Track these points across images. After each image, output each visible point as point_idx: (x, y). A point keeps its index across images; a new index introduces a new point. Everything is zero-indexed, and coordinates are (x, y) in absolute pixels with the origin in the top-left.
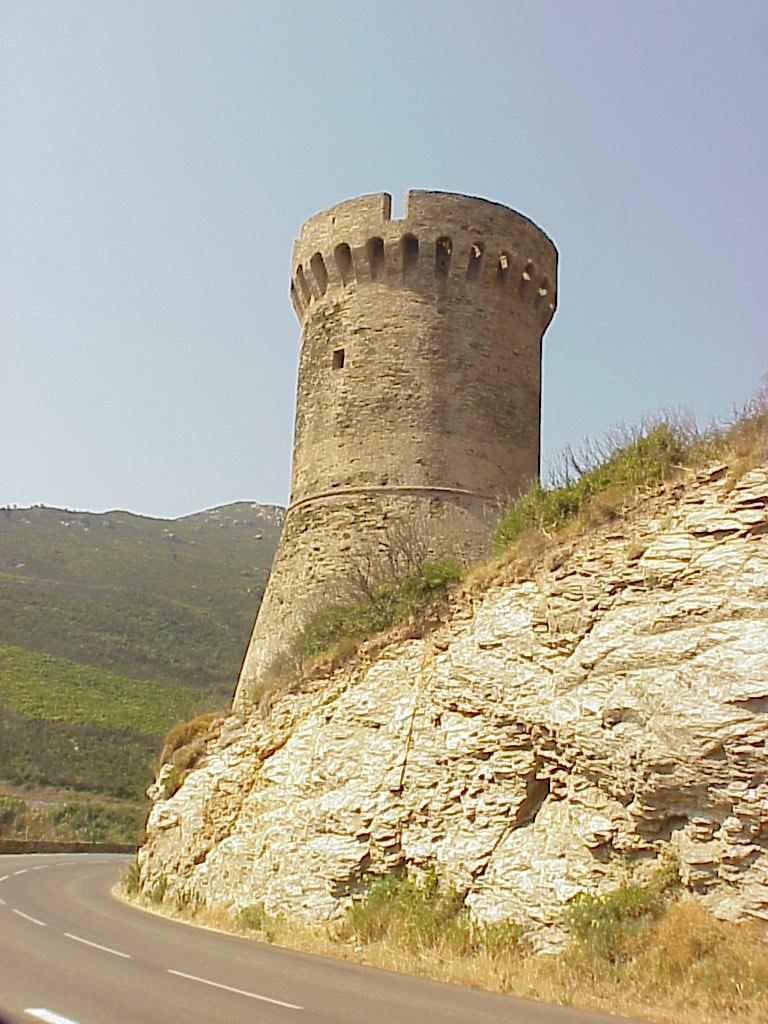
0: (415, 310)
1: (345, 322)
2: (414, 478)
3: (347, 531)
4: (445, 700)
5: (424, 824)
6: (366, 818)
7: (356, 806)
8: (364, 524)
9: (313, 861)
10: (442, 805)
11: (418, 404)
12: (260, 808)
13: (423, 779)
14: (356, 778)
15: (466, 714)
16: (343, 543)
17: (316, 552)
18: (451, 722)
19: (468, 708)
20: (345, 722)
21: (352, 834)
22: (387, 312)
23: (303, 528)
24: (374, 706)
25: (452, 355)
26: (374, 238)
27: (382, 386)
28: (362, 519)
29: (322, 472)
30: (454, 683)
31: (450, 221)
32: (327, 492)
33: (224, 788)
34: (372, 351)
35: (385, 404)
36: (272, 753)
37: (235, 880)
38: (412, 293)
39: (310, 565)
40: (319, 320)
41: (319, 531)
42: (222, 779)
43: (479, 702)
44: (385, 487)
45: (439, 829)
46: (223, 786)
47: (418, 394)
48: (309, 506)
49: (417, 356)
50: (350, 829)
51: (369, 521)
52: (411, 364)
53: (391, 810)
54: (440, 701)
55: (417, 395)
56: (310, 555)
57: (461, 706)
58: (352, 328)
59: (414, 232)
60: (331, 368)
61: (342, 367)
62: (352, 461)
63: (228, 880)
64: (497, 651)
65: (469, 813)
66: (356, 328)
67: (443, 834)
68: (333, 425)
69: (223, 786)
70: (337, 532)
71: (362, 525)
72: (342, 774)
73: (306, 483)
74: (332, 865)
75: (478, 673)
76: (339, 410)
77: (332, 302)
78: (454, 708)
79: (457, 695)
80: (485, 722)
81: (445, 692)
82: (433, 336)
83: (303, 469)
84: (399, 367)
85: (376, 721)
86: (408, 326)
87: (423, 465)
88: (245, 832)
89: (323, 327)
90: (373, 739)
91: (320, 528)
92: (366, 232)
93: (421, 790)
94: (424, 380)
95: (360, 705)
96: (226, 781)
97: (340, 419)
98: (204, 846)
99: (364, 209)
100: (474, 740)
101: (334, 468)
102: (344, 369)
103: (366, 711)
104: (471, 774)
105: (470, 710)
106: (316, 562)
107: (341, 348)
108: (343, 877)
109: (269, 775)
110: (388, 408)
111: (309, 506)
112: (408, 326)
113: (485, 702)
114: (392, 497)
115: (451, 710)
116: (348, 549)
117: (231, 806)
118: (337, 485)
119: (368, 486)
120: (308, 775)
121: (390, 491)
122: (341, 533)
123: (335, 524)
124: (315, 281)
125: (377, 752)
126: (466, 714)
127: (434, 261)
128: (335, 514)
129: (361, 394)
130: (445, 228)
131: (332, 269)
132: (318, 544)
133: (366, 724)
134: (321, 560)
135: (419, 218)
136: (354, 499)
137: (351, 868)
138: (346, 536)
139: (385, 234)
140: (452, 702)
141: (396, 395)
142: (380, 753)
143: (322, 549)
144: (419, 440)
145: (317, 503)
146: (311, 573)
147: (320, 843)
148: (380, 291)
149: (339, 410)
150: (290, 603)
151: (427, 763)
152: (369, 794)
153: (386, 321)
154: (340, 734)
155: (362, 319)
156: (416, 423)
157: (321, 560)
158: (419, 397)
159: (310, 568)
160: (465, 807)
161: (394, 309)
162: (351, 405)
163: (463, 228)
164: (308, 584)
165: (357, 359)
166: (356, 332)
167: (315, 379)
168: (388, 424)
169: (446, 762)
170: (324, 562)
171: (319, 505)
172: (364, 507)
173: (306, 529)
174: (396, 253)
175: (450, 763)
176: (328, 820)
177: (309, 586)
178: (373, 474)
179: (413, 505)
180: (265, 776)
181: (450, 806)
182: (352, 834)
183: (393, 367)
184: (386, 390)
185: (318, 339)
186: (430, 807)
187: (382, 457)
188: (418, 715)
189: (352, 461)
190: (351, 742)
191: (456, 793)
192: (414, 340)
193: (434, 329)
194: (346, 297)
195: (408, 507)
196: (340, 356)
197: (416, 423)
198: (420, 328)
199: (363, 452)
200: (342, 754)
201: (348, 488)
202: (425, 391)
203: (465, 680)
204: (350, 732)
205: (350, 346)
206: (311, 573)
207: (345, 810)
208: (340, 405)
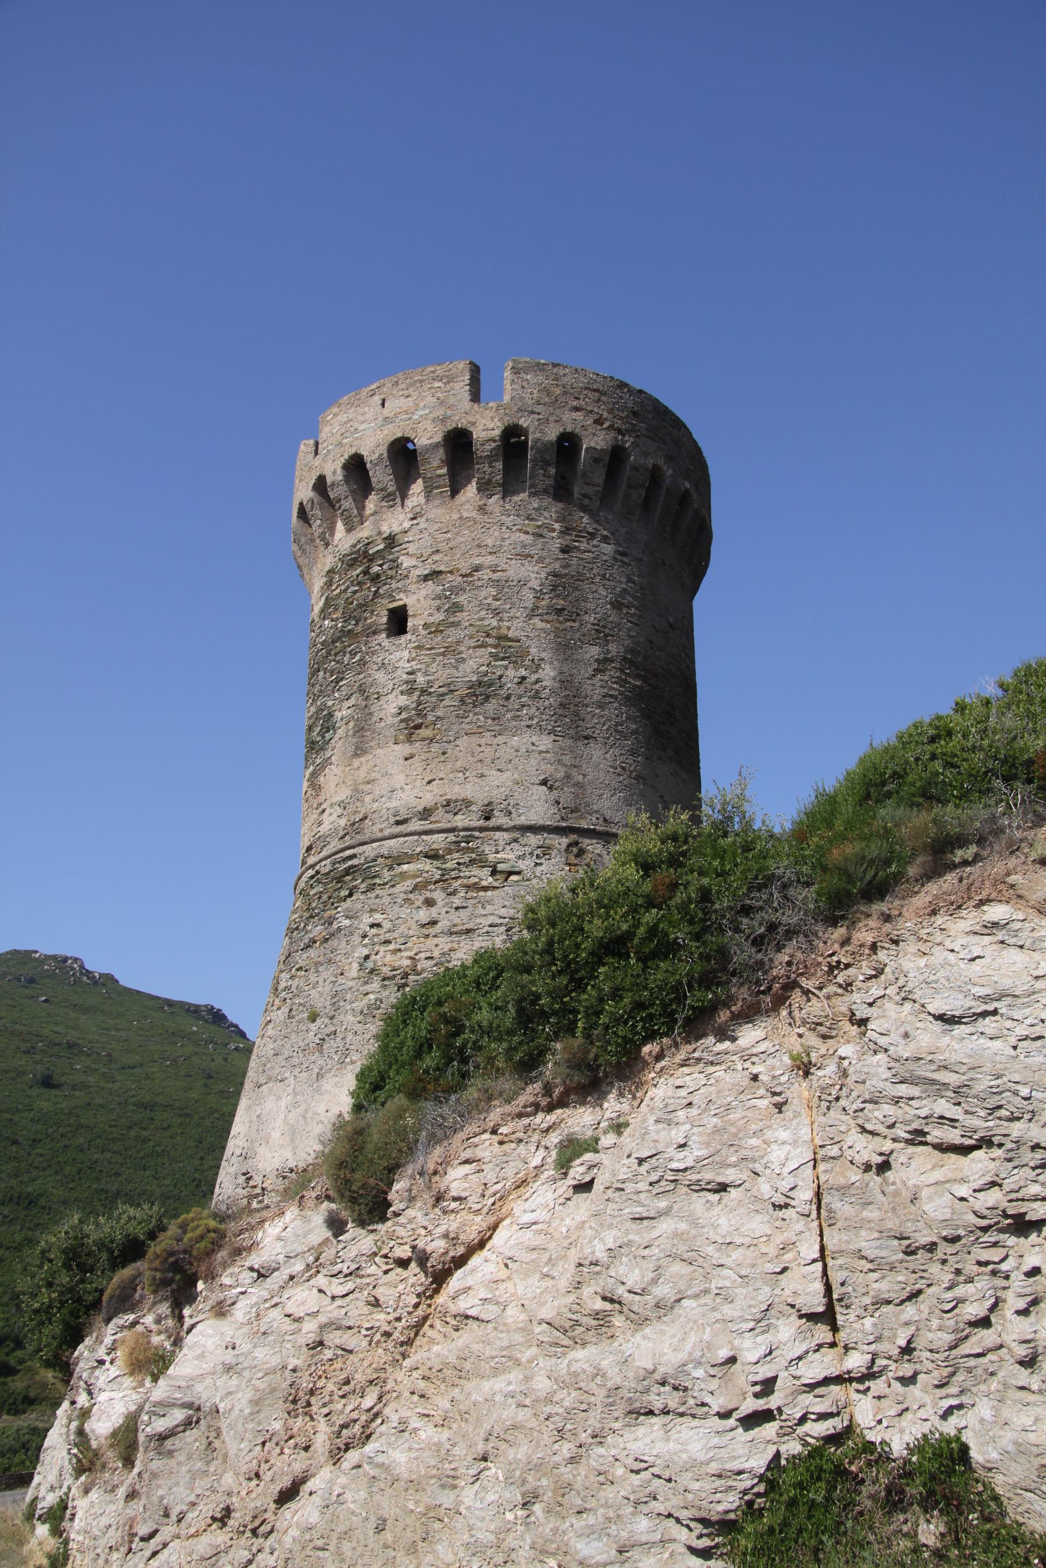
0: (524, 546)
1: (406, 562)
2: (537, 808)
3: (428, 894)
4: (892, 1126)
5: (908, 1381)
6: (759, 1378)
7: (724, 1353)
8: (459, 882)
9: (636, 1480)
10: (948, 1338)
11: (537, 692)
12: (459, 1372)
13: (883, 1286)
14: (696, 1296)
15: (943, 1148)
16: (424, 915)
17: (374, 931)
18: (917, 1168)
19: (953, 1136)
20: (643, 1186)
21: (725, 1415)
22: (479, 546)
23: (344, 893)
24: (704, 1153)
25: (586, 618)
26: (456, 429)
27: (474, 664)
28: (453, 874)
29: (375, 801)
30: (903, 1090)
31: (577, 409)
32: (387, 833)
33: (338, 1341)
34: (457, 608)
35: (481, 691)
36: (460, 1262)
37: (409, 1535)
38: (518, 520)
39: (365, 952)
40: (353, 563)
41: (377, 897)
42: (331, 1324)
43: (980, 1124)
44: (492, 823)
45: (953, 1390)
46: (334, 1338)
47: (537, 676)
48: (354, 856)
49: (530, 617)
50: (717, 1404)
51: (465, 877)
52: (523, 629)
53: (811, 1356)
54: (881, 1129)
55: (534, 677)
56: (364, 936)
57: (937, 1134)
58: (418, 572)
59: (524, 422)
60: (384, 635)
61: (405, 632)
62: (429, 782)
63: (388, 1536)
64: (988, 1025)
65: (1022, 1351)
66: (426, 572)
67: (965, 1399)
68: (393, 725)
69: (334, 1338)
70: (411, 896)
71: (456, 884)
72: (663, 1291)
73: (343, 822)
74: (695, 1486)
75: (964, 1069)
76: (403, 700)
77: (380, 533)
78: (917, 1138)
79: (923, 1113)
80: (1009, 1160)
81: (887, 1109)
82: (554, 588)
83: (335, 800)
84: (504, 631)
85: (720, 1179)
86: (517, 570)
87: (551, 788)
88: (415, 1430)
89: (366, 572)
90: (721, 1218)
91: (378, 891)
92: (444, 420)
93: (885, 1309)
94: (543, 655)
95: (671, 1151)
96: (338, 1328)
97: (404, 716)
98: (298, 1467)
99: (437, 384)
100: (994, 1197)
101: (399, 794)
102: (408, 636)
103: (689, 1163)
104: (1004, 1267)
105: (958, 1141)
106: (377, 948)
107: (401, 603)
108: (727, 1512)
109: (464, 1305)
110: (487, 698)
111: (354, 856)
112: (517, 570)
113: (991, 1124)
114: (503, 837)
115: (909, 1142)
116: (434, 923)
117: (359, 1377)
118: (404, 822)
119: (460, 821)
120: (572, 1298)
121: (499, 829)
122: (419, 898)
123: (409, 884)
124: (350, 499)
125: (739, 1241)
126: (943, 1148)
127: (552, 471)
128: (405, 867)
129: (440, 673)
130: (571, 421)
131: (381, 476)
132: (378, 917)
133: (698, 1187)
134: (387, 942)
135: (530, 402)
136: (438, 841)
137: (745, 1492)
138: (430, 903)
139: (474, 424)
140: (915, 1126)
141: (501, 677)
142: (747, 1241)
143: (387, 925)
144: (543, 748)
145: (369, 850)
146: (370, 965)
147: (646, 1439)
148: (465, 515)
149: (403, 700)
150: (332, 1018)
151: (883, 1254)
152: (751, 1325)
153: (478, 561)
154: (640, 1211)
155: (436, 557)
156: (536, 721)
157: (387, 942)
158: (537, 681)
159: (367, 957)
160: (1008, 1338)
161: (490, 542)
162: (423, 692)
163: (596, 422)
164: (366, 983)
165: (431, 620)
166: (426, 578)
167: (353, 654)
168: (490, 721)
169: (931, 1247)
170: (392, 947)
171: (373, 854)
172: (456, 855)
173: (351, 895)
174: (491, 459)
175: (944, 1248)
176: (656, 1388)
177: (368, 988)
178: (468, 803)
179: (539, 851)
180: (453, 1309)
181: (967, 1337)
182: (725, 1415)
183: (494, 633)
184: (484, 668)
185: (355, 592)
186: (919, 1343)
187: (482, 776)
188: (827, 1159)
189: (429, 782)
190: (665, 1226)
191: (974, 1310)
192: (525, 591)
193: (555, 576)
194: (407, 525)
195: (531, 854)
196: (398, 621)
197: (536, 721)
198: (534, 574)
199: (449, 765)
200: (655, 1250)
201: (425, 825)
202: (548, 673)
203: (933, 1082)
204: (662, 1204)
205: (419, 602)
206: (370, 965)
207: (699, 1364)
208: (402, 693)
